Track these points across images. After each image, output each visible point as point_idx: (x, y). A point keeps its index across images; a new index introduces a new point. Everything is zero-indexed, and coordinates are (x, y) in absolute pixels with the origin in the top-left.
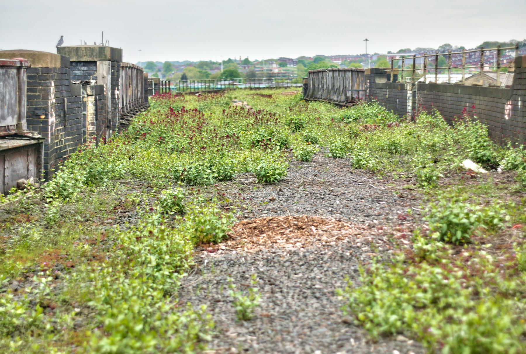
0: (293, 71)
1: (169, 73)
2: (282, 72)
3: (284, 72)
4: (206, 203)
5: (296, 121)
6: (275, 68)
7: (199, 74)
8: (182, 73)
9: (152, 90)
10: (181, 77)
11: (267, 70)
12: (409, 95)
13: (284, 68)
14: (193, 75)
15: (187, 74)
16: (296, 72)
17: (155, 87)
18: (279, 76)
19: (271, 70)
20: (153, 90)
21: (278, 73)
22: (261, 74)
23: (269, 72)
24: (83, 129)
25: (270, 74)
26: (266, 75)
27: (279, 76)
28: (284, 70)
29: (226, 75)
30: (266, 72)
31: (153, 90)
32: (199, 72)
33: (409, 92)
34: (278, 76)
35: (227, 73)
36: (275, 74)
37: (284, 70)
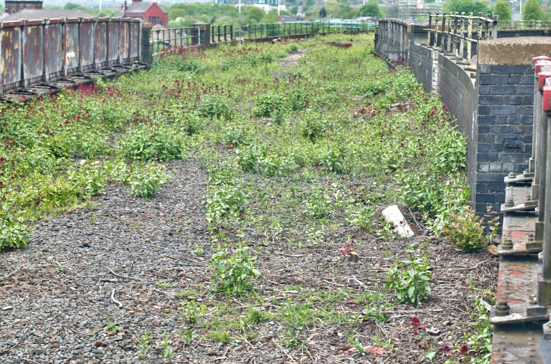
0: (439, 7)
1: (311, 7)
2: (427, 8)
3: (429, 8)
4: (98, 208)
5: (269, 102)
6: (419, 4)
7: (340, 8)
8: (321, 7)
9: (198, 37)
10: (319, 11)
11: (411, 6)
12: (434, 66)
13: (429, 4)
14: (334, 10)
15: (326, 9)
16: (442, 8)
17: (201, 35)
18: (424, 13)
19: (415, 6)
20: (199, 38)
21: (422, 9)
22: (404, 9)
23: (413, 8)
24: (472, 13)
25: (414, 10)
26: (409, 11)
27: (424, 13)
28: (429, 6)
29: (365, 10)
30: (409, 7)
31: (199, 38)
32: (340, 6)
33: (434, 62)
34: (422, 12)
35: (366, 8)
36: (419, 10)
37: (429, 6)
